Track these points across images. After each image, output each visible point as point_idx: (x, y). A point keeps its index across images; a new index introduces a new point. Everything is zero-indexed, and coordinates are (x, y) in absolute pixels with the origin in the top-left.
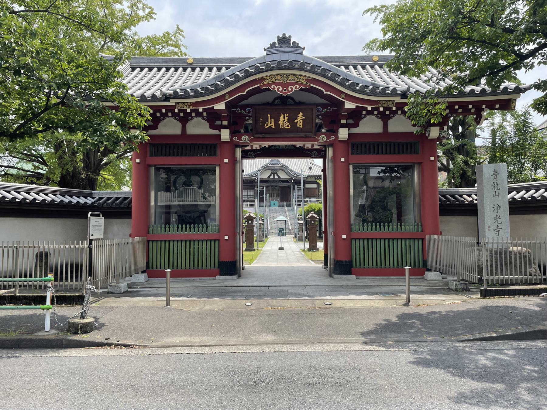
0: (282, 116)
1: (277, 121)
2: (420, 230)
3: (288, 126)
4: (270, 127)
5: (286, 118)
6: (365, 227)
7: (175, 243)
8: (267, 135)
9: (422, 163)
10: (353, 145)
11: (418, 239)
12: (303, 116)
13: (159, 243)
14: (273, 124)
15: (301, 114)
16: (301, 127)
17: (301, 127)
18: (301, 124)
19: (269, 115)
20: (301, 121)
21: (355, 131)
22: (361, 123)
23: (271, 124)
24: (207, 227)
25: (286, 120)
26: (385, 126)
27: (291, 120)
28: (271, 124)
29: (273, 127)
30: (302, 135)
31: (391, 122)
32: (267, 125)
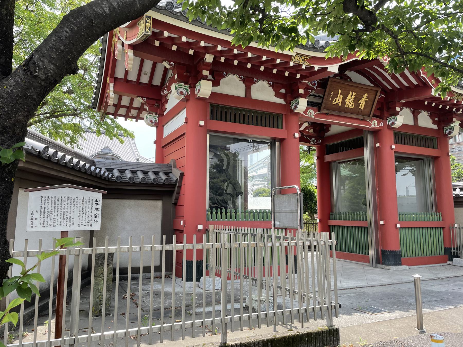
0: (351, 94)
1: (345, 98)
2: (441, 220)
3: (352, 106)
4: (337, 104)
5: (353, 97)
6: (214, 213)
7: (437, 229)
8: (334, 113)
9: (284, 139)
10: (212, 106)
11: (282, 229)
12: (367, 97)
13: (404, 230)
14: (340, 101)
15: (366, 95)
16: (362, 109)
17: (362, 109)
18: (363, 106)
19: (340, 91)
20: (364, 103)
21: (217, 89)
22: (222, 81)
23: (338, 100)
24: (236, 213)
25: (352, 99)
26: (248, 90)
27: (357, 100)
28: (338, 100)
29: (340, 104)
30: (361, 117)
31: (254, 88)
32: (335, 101)
